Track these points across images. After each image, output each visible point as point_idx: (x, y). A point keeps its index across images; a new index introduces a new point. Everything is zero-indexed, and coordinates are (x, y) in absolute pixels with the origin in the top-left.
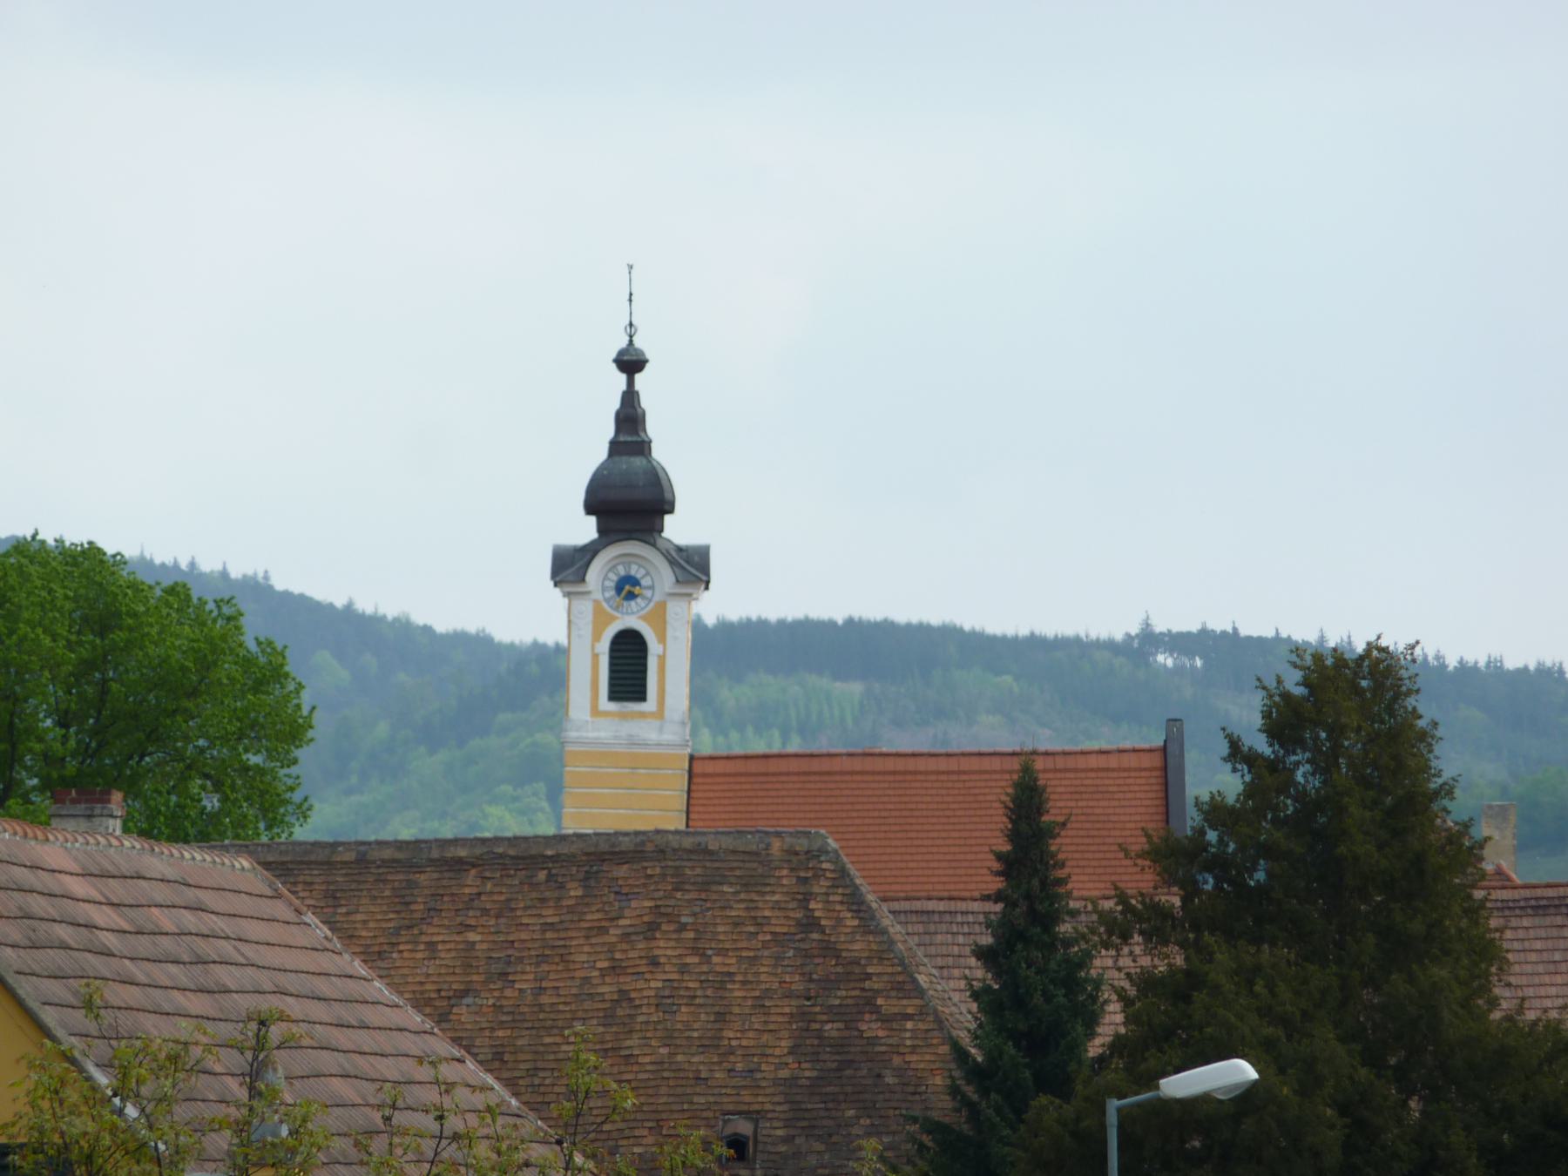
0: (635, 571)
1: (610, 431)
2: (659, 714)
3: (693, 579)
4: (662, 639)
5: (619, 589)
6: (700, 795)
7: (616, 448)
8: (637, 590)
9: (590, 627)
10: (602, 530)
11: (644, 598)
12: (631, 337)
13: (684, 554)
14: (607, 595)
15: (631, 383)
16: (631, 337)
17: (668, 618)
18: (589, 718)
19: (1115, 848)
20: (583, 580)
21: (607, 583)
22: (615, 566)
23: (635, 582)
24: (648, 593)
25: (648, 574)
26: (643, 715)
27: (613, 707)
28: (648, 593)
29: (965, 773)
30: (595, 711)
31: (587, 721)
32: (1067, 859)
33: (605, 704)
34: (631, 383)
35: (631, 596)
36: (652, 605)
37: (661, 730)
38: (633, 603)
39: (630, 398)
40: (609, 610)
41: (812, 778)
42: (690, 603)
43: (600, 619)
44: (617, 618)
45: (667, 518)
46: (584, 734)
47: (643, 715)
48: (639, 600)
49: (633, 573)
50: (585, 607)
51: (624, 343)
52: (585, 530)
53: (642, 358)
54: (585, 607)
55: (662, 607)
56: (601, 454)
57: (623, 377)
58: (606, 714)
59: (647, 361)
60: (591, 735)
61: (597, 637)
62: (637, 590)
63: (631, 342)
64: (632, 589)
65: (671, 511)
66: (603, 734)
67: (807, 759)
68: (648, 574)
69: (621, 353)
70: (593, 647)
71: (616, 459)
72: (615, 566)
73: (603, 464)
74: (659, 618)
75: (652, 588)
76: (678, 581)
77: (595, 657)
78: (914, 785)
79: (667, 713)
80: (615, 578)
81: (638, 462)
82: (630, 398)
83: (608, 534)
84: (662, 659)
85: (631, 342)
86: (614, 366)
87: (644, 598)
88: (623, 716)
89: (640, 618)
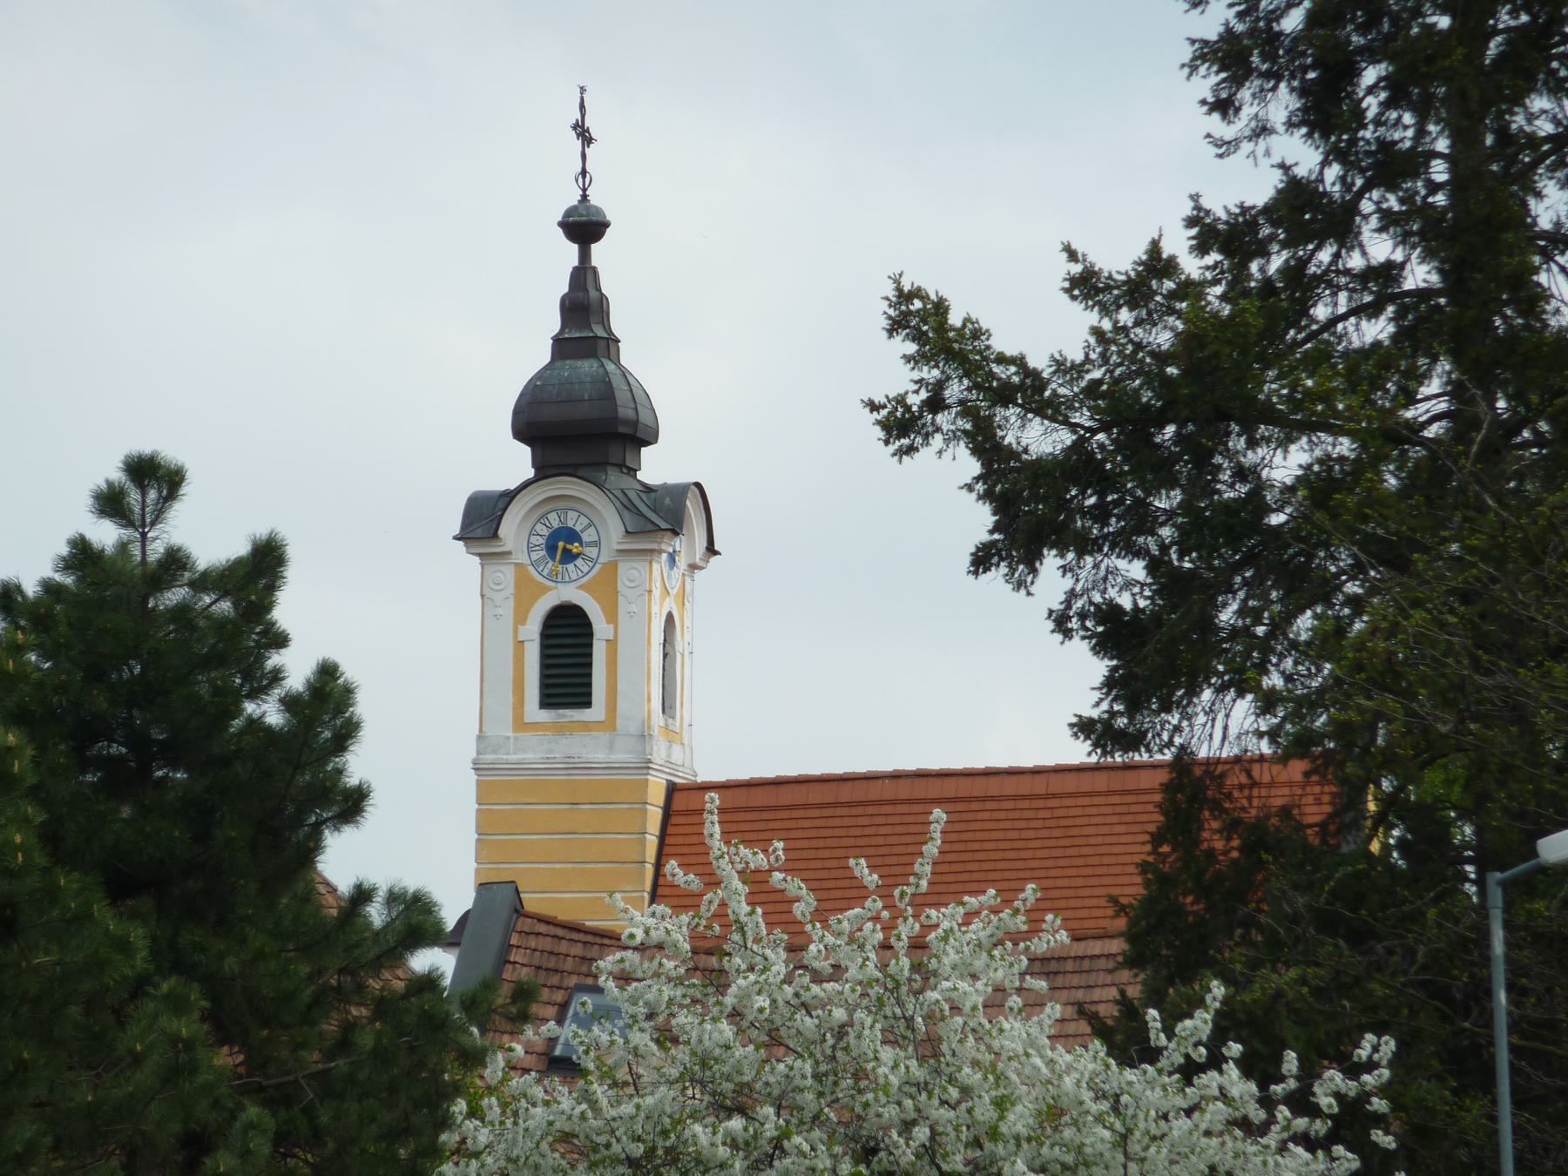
0: (574, 521)
1: (554, 324)
2: (609, 724)
3: (653, 528)
4: (612, 617)
5: (551, 549)
6: (681, 840)
7: (562, 347)
8: (575, 548)
9: (511, 603)
10: (537, 464)
11: (587, 559)
12: (584, 190)
13: (653, 495)
14: (535, 556)
15: (585, 256)
16: (584, 190)
17: (620, 587)
18: (510, 734)
19: (1103, 902)
20: (495, 536)
21: (535, 540)
22: (544, 515)
23: (572, 535)
24: (592, 552)
25: (591, 524)
26: (587, 726)
27: (546, 716)
28: (592, 552)
29: (1054, 796)
30: (520, 724)
31: (508, 738)
32: (1113, 917)
33: (533, 710)
34: (585, 256)
35: (569, 557)
36: (598, 567)
37: (611, 748)
38: (571, 567)
39: (584, 276)
40: (540, 579)
41: (840, 811)
42: (651, 563)
43: (525, 593)
44: (550, 589)
45: (645, 452)
46: (501, 756)
47: (587, 726)
48: (579, 562)
49: (570, 524)
50: (505, 575)
51: (574, 198)
52: (517, 463)
53: (600, 219)
54: (505, 575)
55: (612, 567)
56: (543, 356)
57: (574, 249)
58: (535, 726)
59: (606, 225)
60: (513, 757)
61: (521, 617)
62: (575, 548)
63: (584, 197)
64: (569, 547)
65: (650, 437)
66: (530, 756)
67: (745, 789)
68: (591, 524)
69: (569, 213)
70: (516, 631)
71: (559, 364)
72: (544, 515)
73: (540, 375)
74: (607, 587)
75: (597, 544)
76: (627, 532)
77: (520, 645)
78: (980, 816)
79: (620, 723)
80: (546, 532)
81: (587, 366)
82: (584, 276)
83: (544, 470)
84: (612, 644)
85: (584, 197)
86: (560, 231)
87: (587, 559)
88: (559, 729)
89: (580, 587)
